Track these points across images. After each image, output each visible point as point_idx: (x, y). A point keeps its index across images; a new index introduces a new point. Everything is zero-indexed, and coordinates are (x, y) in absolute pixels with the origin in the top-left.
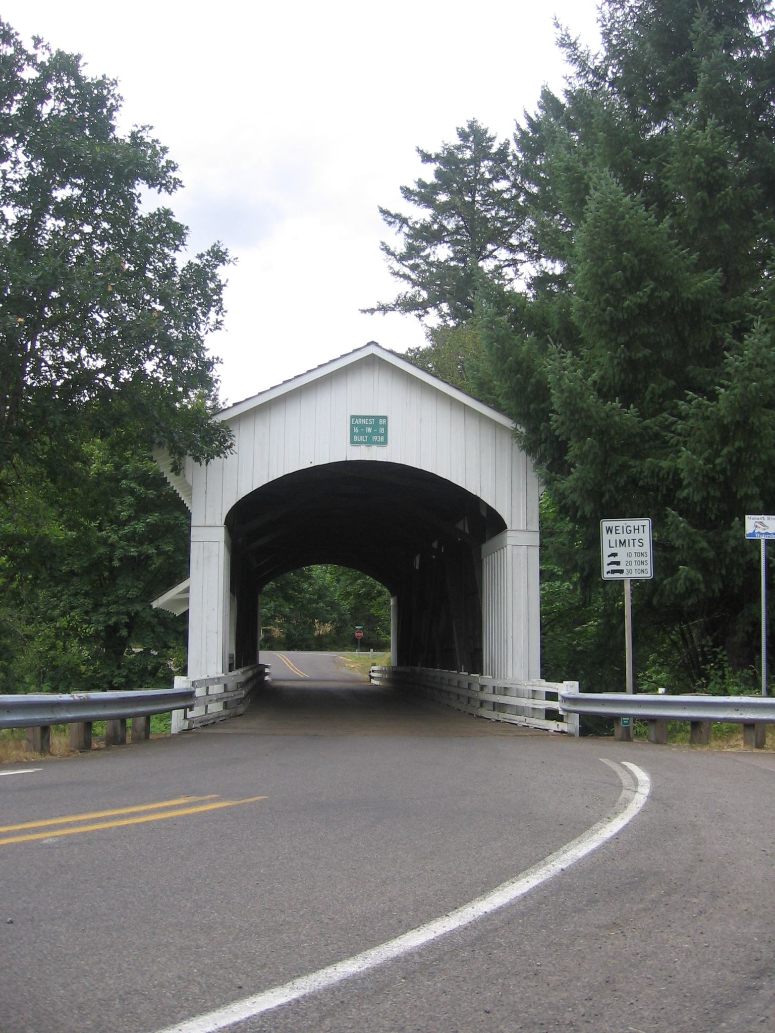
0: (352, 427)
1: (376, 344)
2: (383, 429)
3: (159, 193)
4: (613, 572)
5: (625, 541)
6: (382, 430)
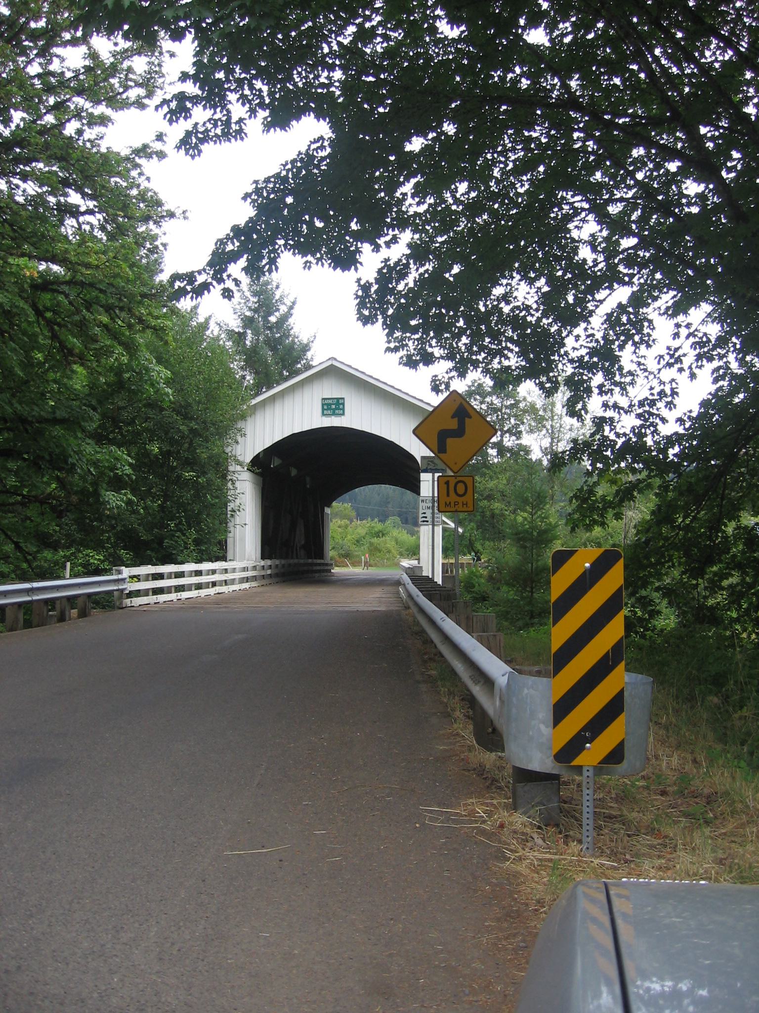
0: (323, 405)
1: (335, 359)
3: (356, 271)
4: (424, 521)
6: (341, 406)
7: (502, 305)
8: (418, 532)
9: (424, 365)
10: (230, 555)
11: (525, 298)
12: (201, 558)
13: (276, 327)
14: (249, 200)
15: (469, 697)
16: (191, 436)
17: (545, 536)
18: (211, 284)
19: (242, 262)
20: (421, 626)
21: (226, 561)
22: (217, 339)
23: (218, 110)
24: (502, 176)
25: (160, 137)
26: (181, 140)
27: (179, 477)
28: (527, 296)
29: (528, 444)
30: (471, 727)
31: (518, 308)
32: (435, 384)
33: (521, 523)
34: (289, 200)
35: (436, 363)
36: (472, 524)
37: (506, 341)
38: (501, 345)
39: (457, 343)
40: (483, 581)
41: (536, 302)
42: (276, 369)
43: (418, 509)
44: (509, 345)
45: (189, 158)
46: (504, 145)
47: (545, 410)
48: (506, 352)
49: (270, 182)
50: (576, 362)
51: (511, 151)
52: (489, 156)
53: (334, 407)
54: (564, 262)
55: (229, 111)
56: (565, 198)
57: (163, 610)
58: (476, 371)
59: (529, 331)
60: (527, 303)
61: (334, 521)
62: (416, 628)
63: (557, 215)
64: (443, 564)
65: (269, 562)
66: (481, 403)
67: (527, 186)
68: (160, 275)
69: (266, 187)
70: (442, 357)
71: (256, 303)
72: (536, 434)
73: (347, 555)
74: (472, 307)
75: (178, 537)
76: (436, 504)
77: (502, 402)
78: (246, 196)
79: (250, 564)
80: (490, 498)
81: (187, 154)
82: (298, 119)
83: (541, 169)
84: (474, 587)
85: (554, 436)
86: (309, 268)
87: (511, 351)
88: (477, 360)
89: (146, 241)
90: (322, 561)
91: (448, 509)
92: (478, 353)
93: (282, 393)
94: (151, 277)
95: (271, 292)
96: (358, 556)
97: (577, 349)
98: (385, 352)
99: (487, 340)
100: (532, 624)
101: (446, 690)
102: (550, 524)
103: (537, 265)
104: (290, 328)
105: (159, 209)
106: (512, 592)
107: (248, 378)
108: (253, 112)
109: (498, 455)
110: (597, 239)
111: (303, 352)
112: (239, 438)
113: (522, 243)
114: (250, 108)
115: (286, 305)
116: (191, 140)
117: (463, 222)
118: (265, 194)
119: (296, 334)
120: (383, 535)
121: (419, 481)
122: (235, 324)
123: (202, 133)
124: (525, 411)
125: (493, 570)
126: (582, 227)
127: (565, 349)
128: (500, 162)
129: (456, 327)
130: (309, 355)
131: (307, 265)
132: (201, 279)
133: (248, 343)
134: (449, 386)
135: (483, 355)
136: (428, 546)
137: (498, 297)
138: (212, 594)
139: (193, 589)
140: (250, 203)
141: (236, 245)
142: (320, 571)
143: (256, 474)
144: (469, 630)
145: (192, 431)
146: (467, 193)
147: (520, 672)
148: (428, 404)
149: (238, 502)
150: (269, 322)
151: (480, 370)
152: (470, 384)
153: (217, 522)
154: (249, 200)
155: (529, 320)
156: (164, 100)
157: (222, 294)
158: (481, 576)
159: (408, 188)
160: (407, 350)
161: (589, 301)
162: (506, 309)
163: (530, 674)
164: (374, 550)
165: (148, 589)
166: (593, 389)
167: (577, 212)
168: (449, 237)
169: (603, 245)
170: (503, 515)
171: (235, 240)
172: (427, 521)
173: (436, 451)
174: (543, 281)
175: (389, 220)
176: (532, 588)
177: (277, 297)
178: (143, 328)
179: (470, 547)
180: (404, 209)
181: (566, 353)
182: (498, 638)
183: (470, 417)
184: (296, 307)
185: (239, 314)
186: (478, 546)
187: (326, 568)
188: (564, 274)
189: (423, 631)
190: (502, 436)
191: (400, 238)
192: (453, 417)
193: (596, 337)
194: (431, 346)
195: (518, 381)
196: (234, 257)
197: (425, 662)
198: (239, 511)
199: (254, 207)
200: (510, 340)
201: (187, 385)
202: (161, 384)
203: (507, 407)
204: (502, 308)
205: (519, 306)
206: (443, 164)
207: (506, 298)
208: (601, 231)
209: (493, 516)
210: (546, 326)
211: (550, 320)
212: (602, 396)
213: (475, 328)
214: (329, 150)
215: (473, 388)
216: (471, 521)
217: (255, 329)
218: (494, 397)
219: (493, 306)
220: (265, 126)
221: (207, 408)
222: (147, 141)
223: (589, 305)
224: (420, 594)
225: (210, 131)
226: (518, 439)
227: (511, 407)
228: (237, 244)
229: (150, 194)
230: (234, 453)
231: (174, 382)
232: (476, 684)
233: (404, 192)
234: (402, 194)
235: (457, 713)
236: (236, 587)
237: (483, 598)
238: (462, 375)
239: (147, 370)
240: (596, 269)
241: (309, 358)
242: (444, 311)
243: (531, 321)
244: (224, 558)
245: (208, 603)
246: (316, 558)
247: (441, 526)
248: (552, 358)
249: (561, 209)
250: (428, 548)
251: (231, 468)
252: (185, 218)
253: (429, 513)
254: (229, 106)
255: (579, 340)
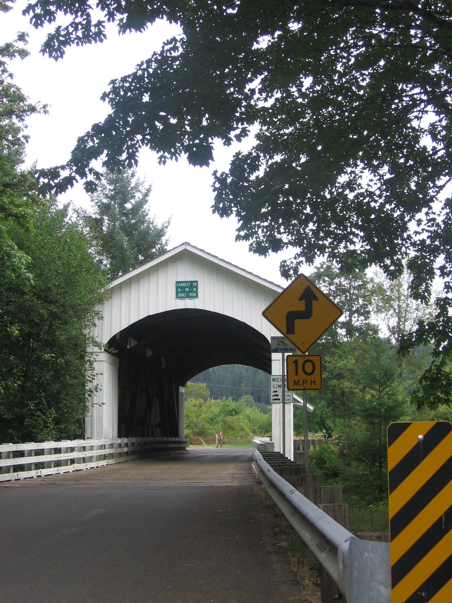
0: (177, 288)
1: (188, 244)
2: (195, 294)
4: (275, 399)
5: (299, 381)
6: (195, 289)
7: (347, 192)
8: (270, 410)
9: (273, 251)
10: (87, 435)
11: (368, 185)
12: (60, 437)
13: (132, 214)
14: (107, 100)
15: (318, 567)
16: (50, 319)
17: (392, 413)
18: (74, 178)
19: (103, 157)
20: (273, 501)
21: (84, 439)
22: (75, 225)
23: (79, 14)
24: (344, 70)
25: (22, 37)
26: (45, 43)
27: (39, 358)
28: (370, 183)
29: (376, 324)
30: (319, 594)
31: (361, 194)
32: (284, 269)
33: (369, 400)
34: (146, 98)
35: (285, 248)
36: (323, 402)
37: (351, 227)
38: (346, 230)
39: (304, 229)
40: (334, 456)
41: (379, 188)
42: (132, 254)
43: (269, 391)
44: (353, 230)
45: (52, 59)
46: (346, 42)
47: (392, 291)
48: (351, 237)
49: (127, 81)
50: (418, 245)
51: (353, 48)
52: (332, 52)
53: (187, 290)
54: (405, 151)
55: (88, 15)
56: (405, 91)
57: (23, 486)
58: (323, 256)
59: (373, 216)
60: (370, 189)
61: (189, 400)
62: (268, 503)
63: (398, 106)
64: (295, 441)
65: (125, 440)
66: (330, 284)
67: (368, 80)
68: (20, 165)
69: (123, 86)
70: (290, 243)
71: (112, 191)
72: (384, 314)
73: (202, 433)
74: (317, 193)
75: (38, 416)
76: (286, 383)
77: (350, 283)
78: (104, 96)
79: (107, 442)
80: (340, 376)
81: (50, 56)
82: (152, 20)
83: (382, 63)
84: (325, 462)
85: (401, 316)
86: (164, 162)
87: (356, 236)
88: (324, 245)
89: (8, 134)
90: (177, 439)
91: (297, 387)
92: (325, 238)
93: (138, 277)
94: (12, 167)
95: (126, 180)
96: (212, 434)
97: (419, 233)
98: (236, 240)
99: (333, 226)
100: (381, 498)
101: (296, 560)
102: (396, 401)
103: (380, 153)
104: (145, 214)
105: (21, 104)
106: (361, 467)
107: (105, 262)
108: (111, 16)
109: (347, 335)
110: (437, 128)
111: (158, 237)
112: (97, 321)
113: (365, 133)
114: (108, 11)
115: (141, 192)
116: (54, 43)
117: (309, 114)
118: (122, 93)
119: (151, 220)
120: (236, 413)
121: (270, 360)
122: (92, 211)
123: (63, 36)
124: (373, 292)
125: (344, 446)
126: (421, 117)
127: (408, 233)
128: (343, 57)
129: (303, 214)
130: (164, 239)
131: (162, 161)
132: (64, 174)
133: (104, 228)
134: (298, 271)
135: (330, 240)
136: (280, 423)
137: (343, 185)
138: (71, 471)
139: (53, 466)
140: (109, 102)
141: (96, 142)
142: (174, 449)
143: (113, 354)
144: (316, 502)
145: (51, 314)
146: (312, 87)
147: (361, 537)
148: (279, 286)
149: (95, 382)
150: (125, 208)
151: (326, 255)
152: (319, 266)
153: (75, 402)
154: (107, 100)
155: (372, 206)
156: (30, 5)
157: (85, 188)
158: (333, 452)
159: (256, 84)
160: (256, 238)
161: (430, 188)
162: (351, 196)
163: (371, 539)
164: (228, 428)
165: (9, 466)
166: (435, 270)
167: (415, 103)
168: (296, 128)
169: (444, 133)
170: (352, 393)
171: (95, 138)
172: (279, 399)
173: (285, 332)
174: (386, 168)
175: (238, 115)
176: (380, 463)
177: (133, 185)
178: (6, 216)
179: (322, 425)
180: (252, 102)
181: (409, 237)
182: (343, 508)
183: (317, 299)
184: (151, 194)
185: (96, 201)
186: (329, 423)
187: (181, 445)
188: (406, 161)
189: (275, 505)
190: (350, 316)
191: (249, 131)
192: (300, 299)
193: (437, 221)
194: (279, 233)
195: (364, 264)
196: (95, 153)
197: (276, 534)
198: (97, 391)
199: (112, 105)
200: (356, 226)
201: (47, 271)
202: (23, 270)
203: (355, 288)
204: (347, 195)
205: (363, 193)
206: (289, 60)
207: (350, 185)
208: (440, 121)
209: (343, 394)
210: (389, 212)
211: (393, 206)
212: (444, 278)
213: (321, 214)
214: (181, 50)
215: (322, 270)
216: (321, 399)
217: (111, 216)
218: (343, 279)
219: (338, 193)
220: (121, 27)
221: (66, 292)
222: (10, 40)
223: (430, 191)
224: (271, 469)
225: (72, 34)
226: (366, 319)
227: (359, 287)
228: (96, 141)
229: (13, 89)
230: (91, 335)
231: (34, 267)
232: (322, 551)
233: (252, 87)
234: (249, 90)
235: (307, 581)
236: (94, 464)
237: (334, 474)
238: (310, 260)
239: (9, 256)
240: (436, 157)
241: (164, 243)
242: (291, 199)
243: (375, 207)
244: (82, 436)
245: (68, 480)
246: (171, 436)
247: (292, 404)
248: (396, 242)
249: (401, 101)
250: (280, 425)
251: (89, 350)
252: (46, 112)
253: (280, 393)
254: (89, 11)
255: (421, 224)
